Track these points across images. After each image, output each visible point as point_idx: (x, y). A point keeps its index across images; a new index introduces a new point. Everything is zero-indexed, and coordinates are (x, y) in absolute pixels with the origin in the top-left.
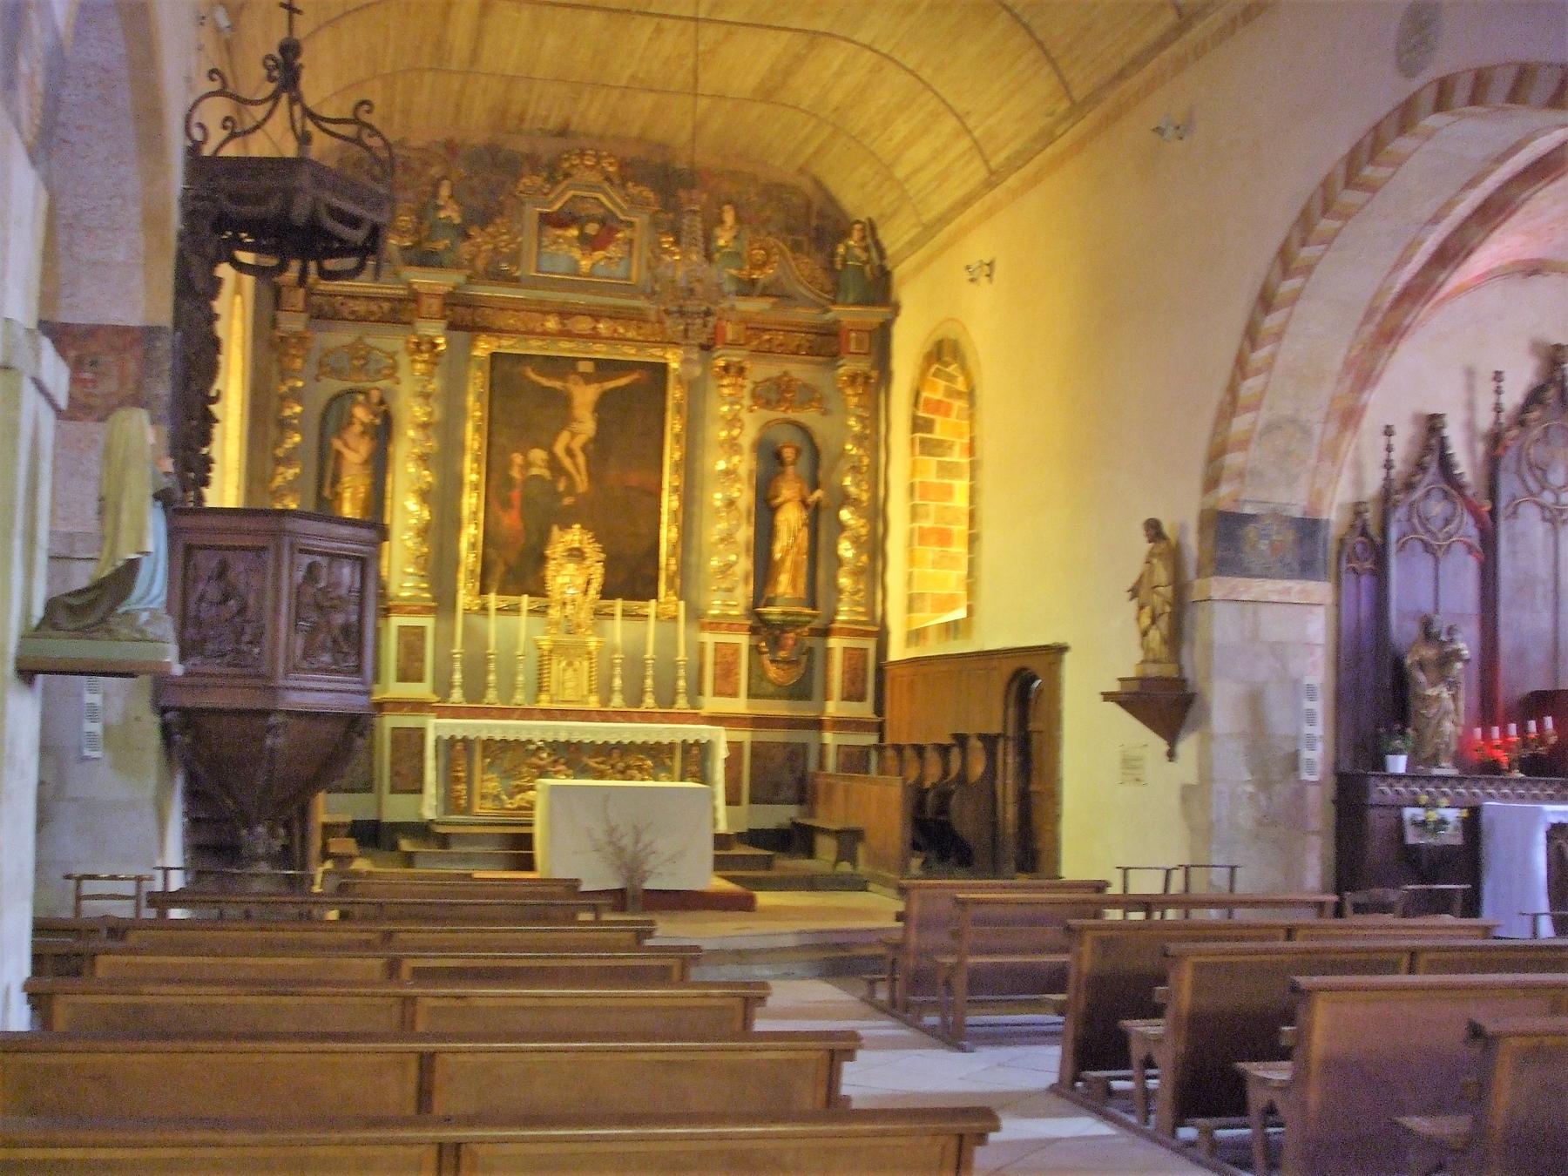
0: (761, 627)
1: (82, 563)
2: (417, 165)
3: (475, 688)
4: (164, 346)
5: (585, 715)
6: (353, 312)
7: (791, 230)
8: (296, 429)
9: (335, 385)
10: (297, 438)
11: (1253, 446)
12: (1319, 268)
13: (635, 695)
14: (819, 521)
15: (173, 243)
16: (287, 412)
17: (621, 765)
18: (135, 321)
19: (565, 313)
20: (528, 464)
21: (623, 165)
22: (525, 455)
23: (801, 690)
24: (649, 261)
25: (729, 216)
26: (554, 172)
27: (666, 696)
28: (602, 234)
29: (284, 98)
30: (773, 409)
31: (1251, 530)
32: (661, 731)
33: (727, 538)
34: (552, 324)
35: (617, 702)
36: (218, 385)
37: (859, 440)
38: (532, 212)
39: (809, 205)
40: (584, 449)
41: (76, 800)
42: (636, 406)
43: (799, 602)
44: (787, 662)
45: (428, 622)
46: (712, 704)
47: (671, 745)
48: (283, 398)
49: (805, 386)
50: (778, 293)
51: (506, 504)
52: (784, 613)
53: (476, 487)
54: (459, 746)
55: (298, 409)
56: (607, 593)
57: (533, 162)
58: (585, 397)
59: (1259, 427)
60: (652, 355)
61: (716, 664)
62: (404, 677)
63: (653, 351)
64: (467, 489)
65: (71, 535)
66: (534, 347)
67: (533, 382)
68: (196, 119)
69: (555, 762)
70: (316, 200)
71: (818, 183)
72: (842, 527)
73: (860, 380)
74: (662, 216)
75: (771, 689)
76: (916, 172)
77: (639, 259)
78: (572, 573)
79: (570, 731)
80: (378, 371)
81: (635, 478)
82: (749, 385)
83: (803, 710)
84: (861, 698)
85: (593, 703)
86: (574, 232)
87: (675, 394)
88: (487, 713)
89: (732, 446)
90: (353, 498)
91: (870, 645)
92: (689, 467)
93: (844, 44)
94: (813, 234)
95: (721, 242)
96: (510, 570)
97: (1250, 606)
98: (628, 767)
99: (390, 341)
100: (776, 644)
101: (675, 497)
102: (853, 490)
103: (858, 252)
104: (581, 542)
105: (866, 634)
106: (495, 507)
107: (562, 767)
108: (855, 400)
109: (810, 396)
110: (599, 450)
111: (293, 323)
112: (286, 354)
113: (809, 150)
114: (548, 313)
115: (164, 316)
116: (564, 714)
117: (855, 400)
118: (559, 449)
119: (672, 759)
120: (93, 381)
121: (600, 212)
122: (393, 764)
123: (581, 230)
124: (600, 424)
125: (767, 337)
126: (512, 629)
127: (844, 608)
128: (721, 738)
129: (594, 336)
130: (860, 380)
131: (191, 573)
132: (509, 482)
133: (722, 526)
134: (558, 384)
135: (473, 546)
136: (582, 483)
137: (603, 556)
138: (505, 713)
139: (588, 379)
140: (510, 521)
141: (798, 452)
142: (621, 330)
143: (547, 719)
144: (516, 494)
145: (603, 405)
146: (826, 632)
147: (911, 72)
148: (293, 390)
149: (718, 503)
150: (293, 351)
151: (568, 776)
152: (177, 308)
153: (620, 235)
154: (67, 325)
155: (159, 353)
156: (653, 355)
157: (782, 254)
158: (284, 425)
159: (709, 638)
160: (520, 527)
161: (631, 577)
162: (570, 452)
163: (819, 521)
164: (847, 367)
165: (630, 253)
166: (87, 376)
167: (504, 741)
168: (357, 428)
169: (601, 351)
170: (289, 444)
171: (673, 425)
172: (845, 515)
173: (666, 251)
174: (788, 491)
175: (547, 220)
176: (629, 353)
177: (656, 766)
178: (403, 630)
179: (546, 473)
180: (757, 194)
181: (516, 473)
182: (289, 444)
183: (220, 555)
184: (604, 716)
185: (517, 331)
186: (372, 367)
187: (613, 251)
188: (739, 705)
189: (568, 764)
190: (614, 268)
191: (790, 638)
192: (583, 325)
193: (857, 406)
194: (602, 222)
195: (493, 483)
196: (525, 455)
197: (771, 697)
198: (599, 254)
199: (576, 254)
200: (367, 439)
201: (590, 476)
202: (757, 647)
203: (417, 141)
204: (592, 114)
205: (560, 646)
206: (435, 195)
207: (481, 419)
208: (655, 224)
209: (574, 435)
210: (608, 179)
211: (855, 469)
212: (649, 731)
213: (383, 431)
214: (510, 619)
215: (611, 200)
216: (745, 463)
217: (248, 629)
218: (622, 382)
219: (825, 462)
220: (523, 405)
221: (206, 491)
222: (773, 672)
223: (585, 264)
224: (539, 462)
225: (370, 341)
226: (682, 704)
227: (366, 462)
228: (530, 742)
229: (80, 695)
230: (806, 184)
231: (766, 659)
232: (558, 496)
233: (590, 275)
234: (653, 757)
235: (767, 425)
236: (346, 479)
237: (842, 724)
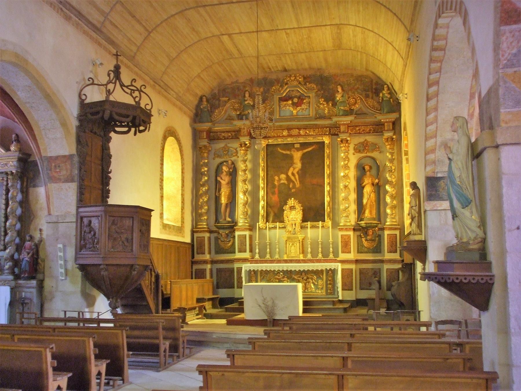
0: (360, 230)
2: (242, 88)
3: (262, 254)
4: (76, 159)
5: (298, 261)
6: (224, 137)
7: (365, 90)
8: (205, 175)
9: (218, 160)
11: (437, 151)
12: (440, 82)
13: (314, 253)
14: (378, 188)
16: (203, 170)
17: (305, 278)
18: (67, 153)
19: (289, 129)
20: (280, 180)
21: (305, 78)
22: (279, 177)
23: (378, 249)
24: (315, 108)
25: (340, 90)
26: (282, 83)
27: (325, 254)
28: (300, 101)
30: (362, 153)
31: (442, 183)
32: (318, 266)
33: (346, 199)
34: (285, 133)
35: (309, 256)
36: (110, 168)
37: (391, 161)
38: (276, 98)
39: (372, 81)
40: (298, 173)
41: (61, 291)
42: (314, 157)
43: (374, 219)
44: (371, 240)
45: (247, 233)
46: (342, 256)
47: (322, 271)
48: (202, 166)
49: (373, 143)
50: (359, 114)
51: (273, 193)
52: (365, 223)
53: (263, 188)
54: (253, 273)
55: (206, 169)
56: (305, 219)
57: (278, 81)
58: (297, 156)
59: (438, 143)
60: (318, 139)
61: (342, 242)
62: (240, 251)
63: (319, 138)
64: (261, 189)
65: (58, 216)
66: (280, 141)
67: (280, 152)
68: (83, 93)
69: (284, 277)
70: (111, 112)
71: (373, 73)
72: (386, 192)
73: (389, 139)
74: (319, 92)
75: (366, 250)
76: (391, 64)
77: (312, 108)
78: (294, 215)
79: (287, 267)
80: (232, 154)
81: (315, 181)
82: (352, 146)
83: (378, 257)
84: (395, 252)
85: (301, 257)
86: (290, 102)
87: (327, 151)
88: (266, 262)
89: (346, 167)
90: (225, 195)
91: (397, 232)
92: (333, 175)
93: (348, 26)
94: (374, 91)
95: (338, 99)
96: (275, 215)
97: (443, 212)
98: (308, 278)
99: (234, 145)
100: (366, 234)
101: (328, 186)
102: (389, 178)
103: (386, 95)
104: (294, 204)
105: (396, 229)
106: (270, 195)
107: (286, 279)
108: (388, 147)
109: (375, 147)
110: (303, 173)
111: (204, 142)
113: (364, 63)
114: (284, 129)
115: (74, 152)
116: (291, 261)
117: (388, 147)
118: (290, 174)
119: (323, 275)
120: (60, 172)
121: (298, 94)
122: (237, 280)
123: (292, 101)
124: (303, 164)
125: (357, 129)
126: (276, 234)
127: (388, 220)
128: (339, 267)
129: (299, 135)
130: (389, 139)
132: (274, 186)
133: (343, 195)
134: (288, 152)
135: (263, 207)
136: (298, 185)
137: (302, 208)
138: (272, 262)
139: (298, 150)
140: (275, 198)
141: (371, 167)
142: (308, 132)
143: (297, 263)
144: (276, 190)
145: (303, 158)
146: (383, 229)
148: (204, 163)
149: (341, 187)
151: (288, 282)
152: (77, 148)
153: (305, 101)
155: (74, 162)
156: (319, 139)
157: (361, 99)
158: (203, 174)
159: (340, 233)
161: (313, 214)
162: (293, 174)
163: (378, 188)
164: (387, 135)
165: (309, 106)
166: (58, 170)
167: (266, 270)
168: (225, 173)
169: (302, 140)
170: (203, 180)
171: (327, 162)
172: (387, 187)
173: (321, 104)
174: (367, 181)
175: (282, 99)
176: (311, 140)
177: (317, 278)
178: (239, 236)
179: (286, 182)
180: (354, 80)
181: (276, 183)
182: (203, 180)
184: (304, 261)
185: (274, 137)
186: (230, 153)
187: (304, 106)
188: (351, 256)
189: (288, 278)
190: (304, 112)
191: (370, 232)
192: (295, 132)
193: (390, 149)
194: (299, 98)
195: (269, 187)
196: (279, 177)
197: (366, 252)
198: (299, 108)
199: (291, 109)
200: (228, 177)
201: (300, 181)
202: (360, 235)
203: (241, 80)
204: (289, 63)
205: (289, 238)
206: (245, 96)
207: (264, 166)
208: (317, 95)
209: (294, 169)
210: (300, 83)
211: (391, 171)
212: (314, 266)
213: (233, 174)
214: (273, 231)
215: (302, 90)
216: (352, 173)
217: (96, 241)
218: (310, 149)
219: (381, 169)
220: (276, 159)
221: (108, 200)
222: (365, 244)
223: (295, 112)
224: (283, 179)
225: (229, 145)
226: (331, 256)
227: (228, 183)
228: (274, 271)
229: (58, 261)
230: (369, 73)
231: (363, 240)
232: (290, 189)
233: (297, 115)
234: (316, 275)
235: (360, 159)
236: (222, 190)
237: (390, 261)
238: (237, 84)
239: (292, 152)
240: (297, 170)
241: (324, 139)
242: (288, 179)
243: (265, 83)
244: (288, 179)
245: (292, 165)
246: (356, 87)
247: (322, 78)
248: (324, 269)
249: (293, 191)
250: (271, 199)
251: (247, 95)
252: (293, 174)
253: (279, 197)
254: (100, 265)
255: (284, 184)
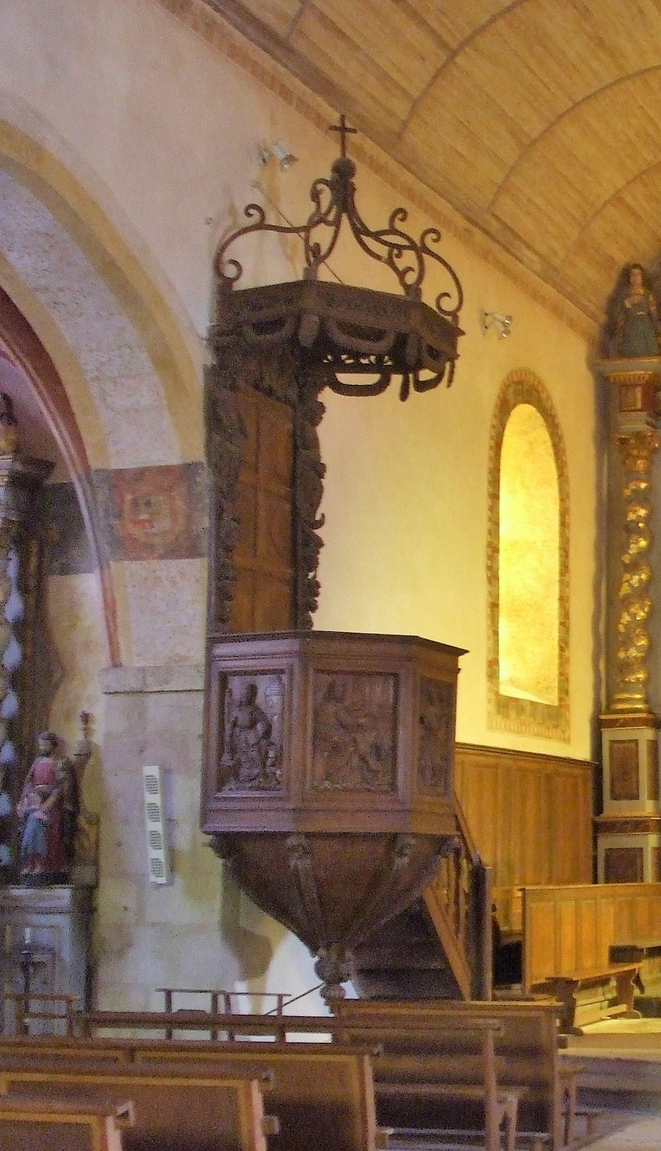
1: (154, 696)
4: (205, 479)
8: (640, 533)
10: (643, 543)
15: (197, 383)
16: (632, 517)
18: (174, 459)
29: (344, 217)
55: (642, 512)
68: (227, 256)
70: (323, 321)
112: (628, 455)
115: (199, 454)
120: (150, 521)
131: (227, 700)
147: (618, 81)
148: (636, 491)
150: (635, 452)
152: (209, 441)
154: (120, 471)
158: (631, 529)
166: (144, 517)
183: (249, 679)
217: (271, 754)
221: (314, 616)
229: (143, 823)
237: (640, 826)
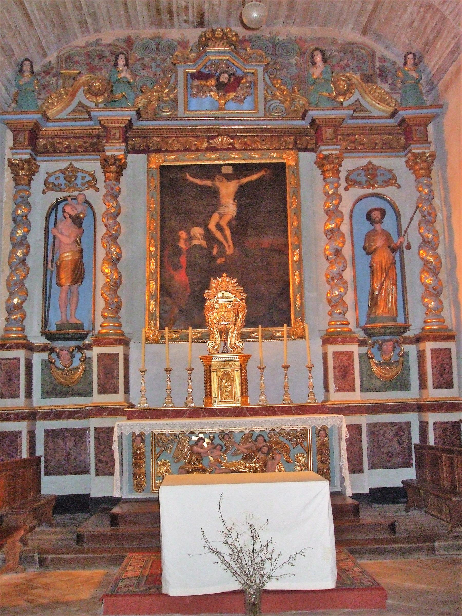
20: (190, 238)
22: (188, 233)
40: (229, 224)
51: (176, 267)
58: (228, 190)
61: (334, 368)
62: (102, 391)
67: (191, 183)
86: (212, 82)
110: (240, 227)
118: (212, 226)
124: (239, 206)
132: (178, 252)
134: (208, 183)
139: (229, 177)
144: (183, 260)
145: (240, 194)
156: (274, 158)
160: (188, 281)
161: (271, 308)
162: (219, 227)
169: (237, 158)
176: (256, 158)
179: (204, 243)
180: (338, 51)
181: (182, 245)
196: (188, 233)
201: (234, 243)
209: (221, 216)
218: (254, 177)
232: (214, 259)
238: (98, 48)
239: (217, 183)
240: (227, 219)
241: (285, 156)
242: (209, 237)
243: (158, 49)
244: (209, 237)
245: (190, 248)
246: (343, 63)
247: (275, 46)
248: (309, 427)
249: (219, 261)
250: (172, 278)
251: (121, 61)
252: (219, 227)
253: (189, 274)
254: (116, 501)
255: (200, 247)
